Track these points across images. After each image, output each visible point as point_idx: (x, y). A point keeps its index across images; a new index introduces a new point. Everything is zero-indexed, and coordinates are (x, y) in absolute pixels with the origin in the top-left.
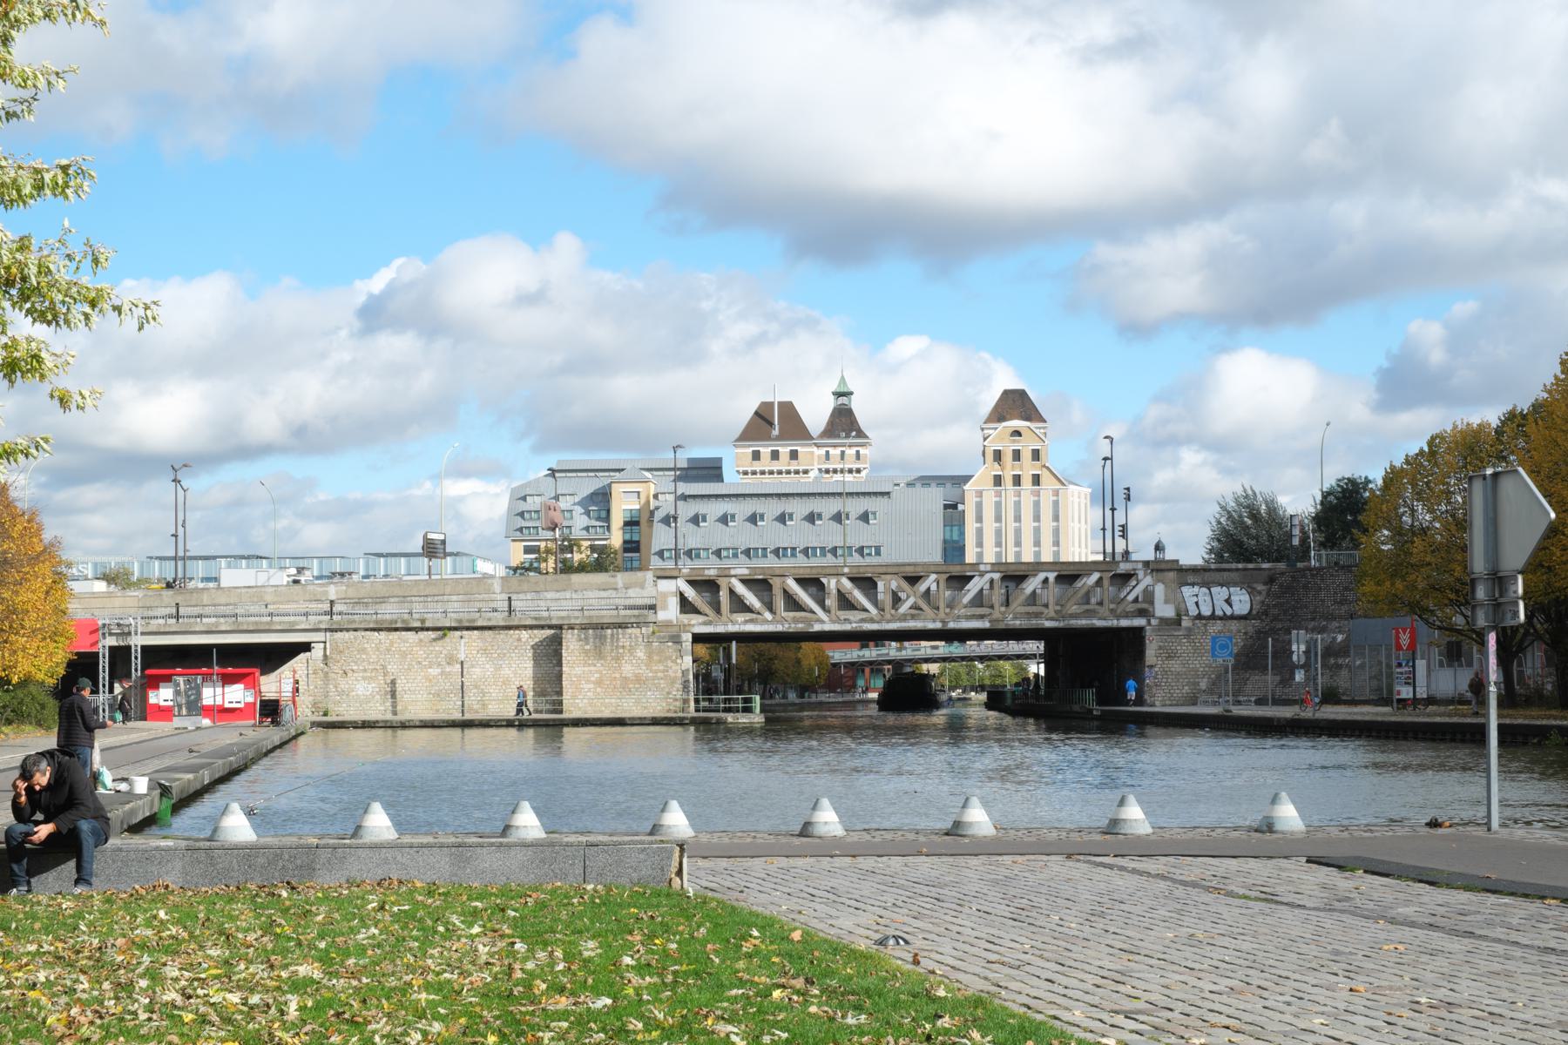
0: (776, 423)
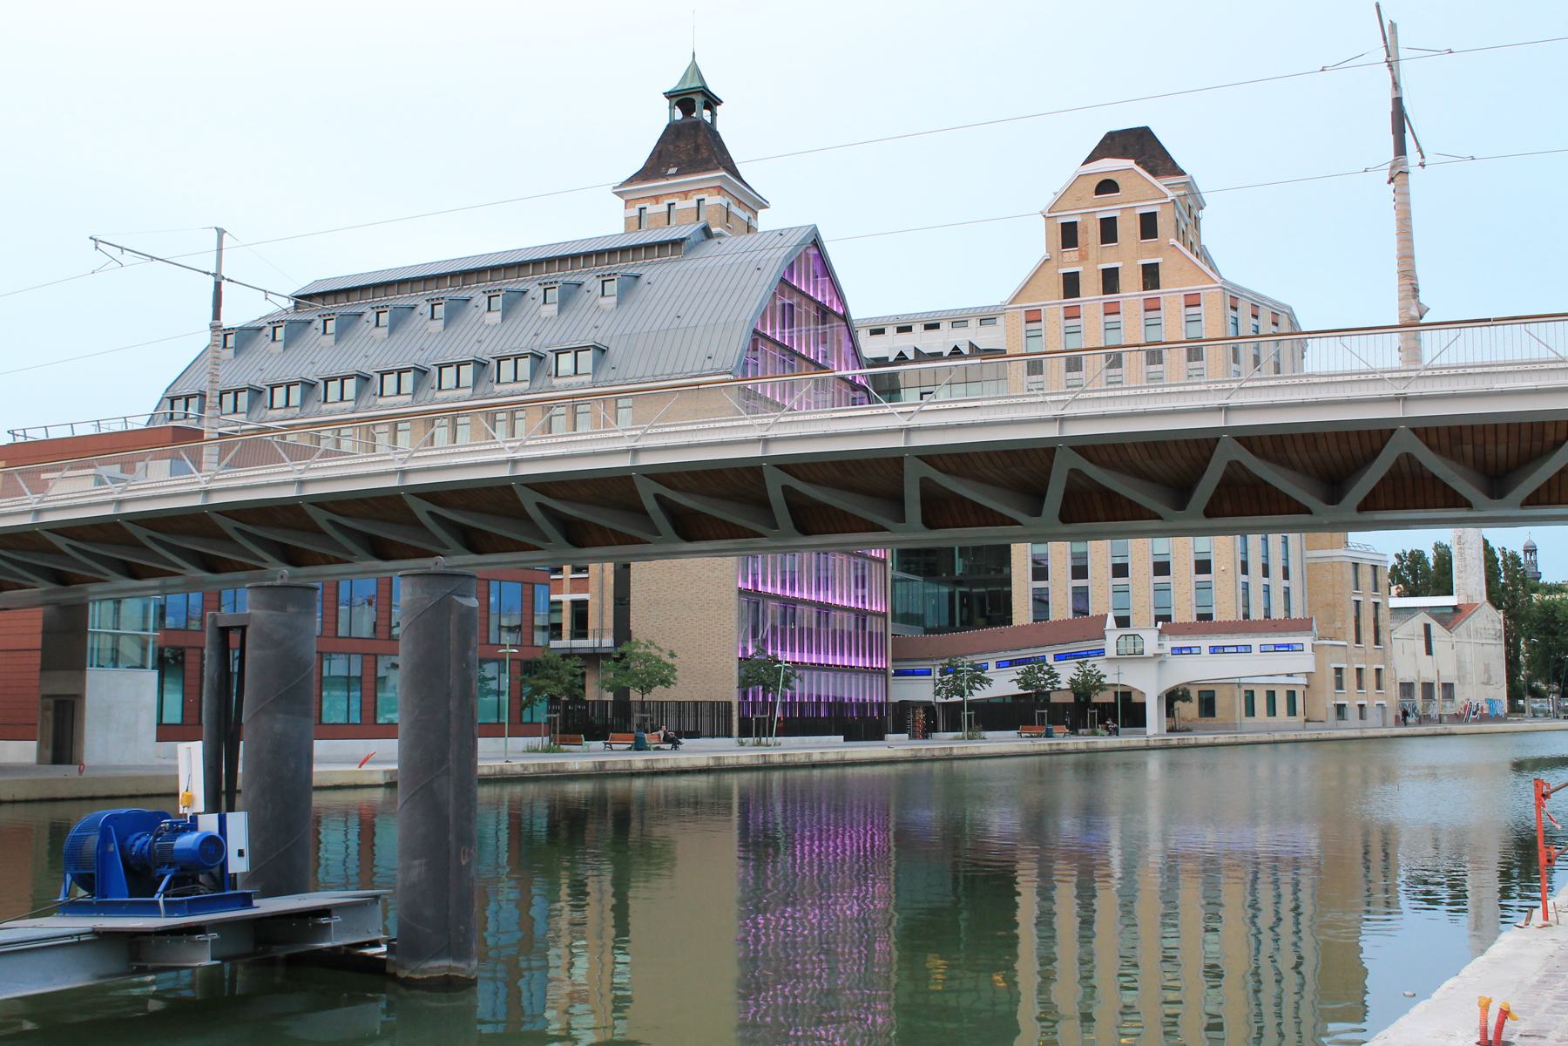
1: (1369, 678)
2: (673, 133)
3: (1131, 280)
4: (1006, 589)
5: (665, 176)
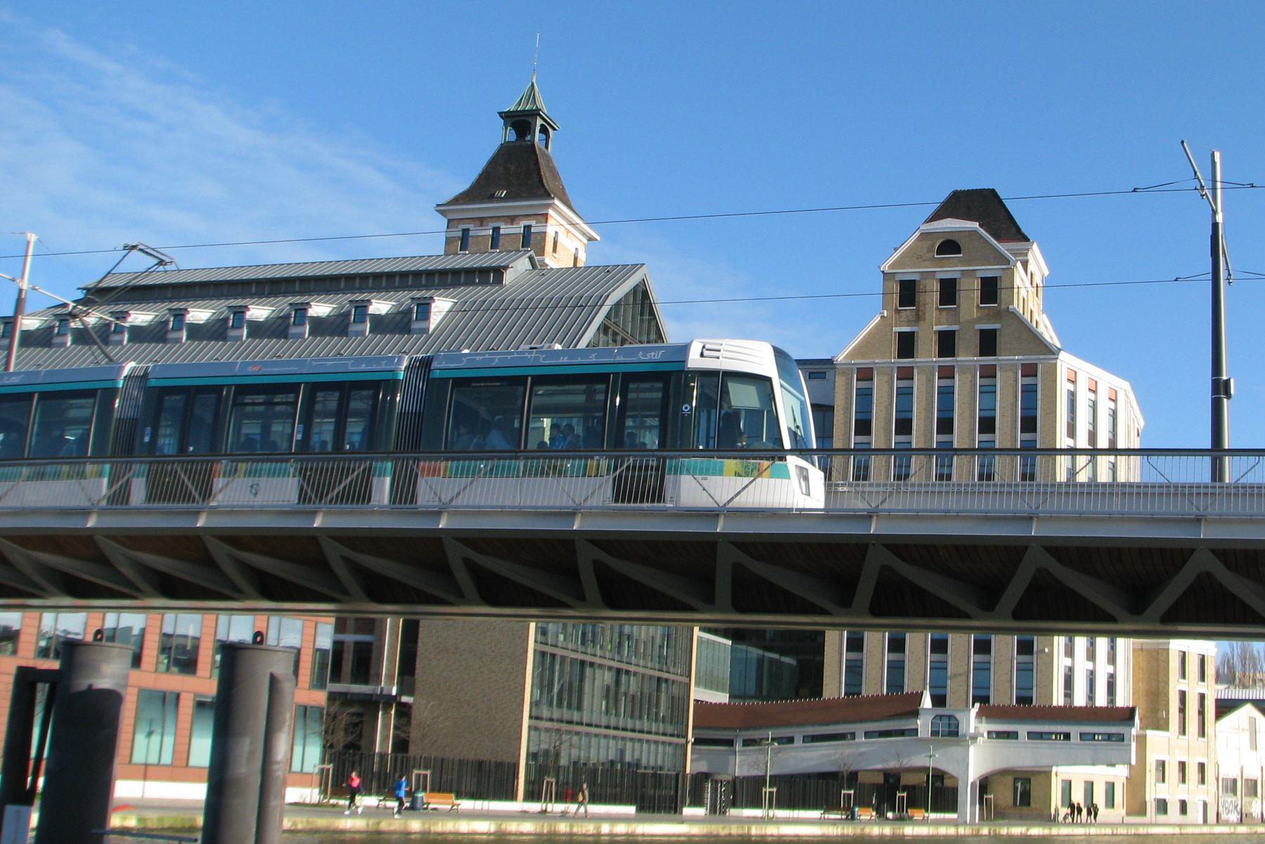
1: (1192, 772)
2: (505, 155)
4: (817, 658)
5: (491, 198)
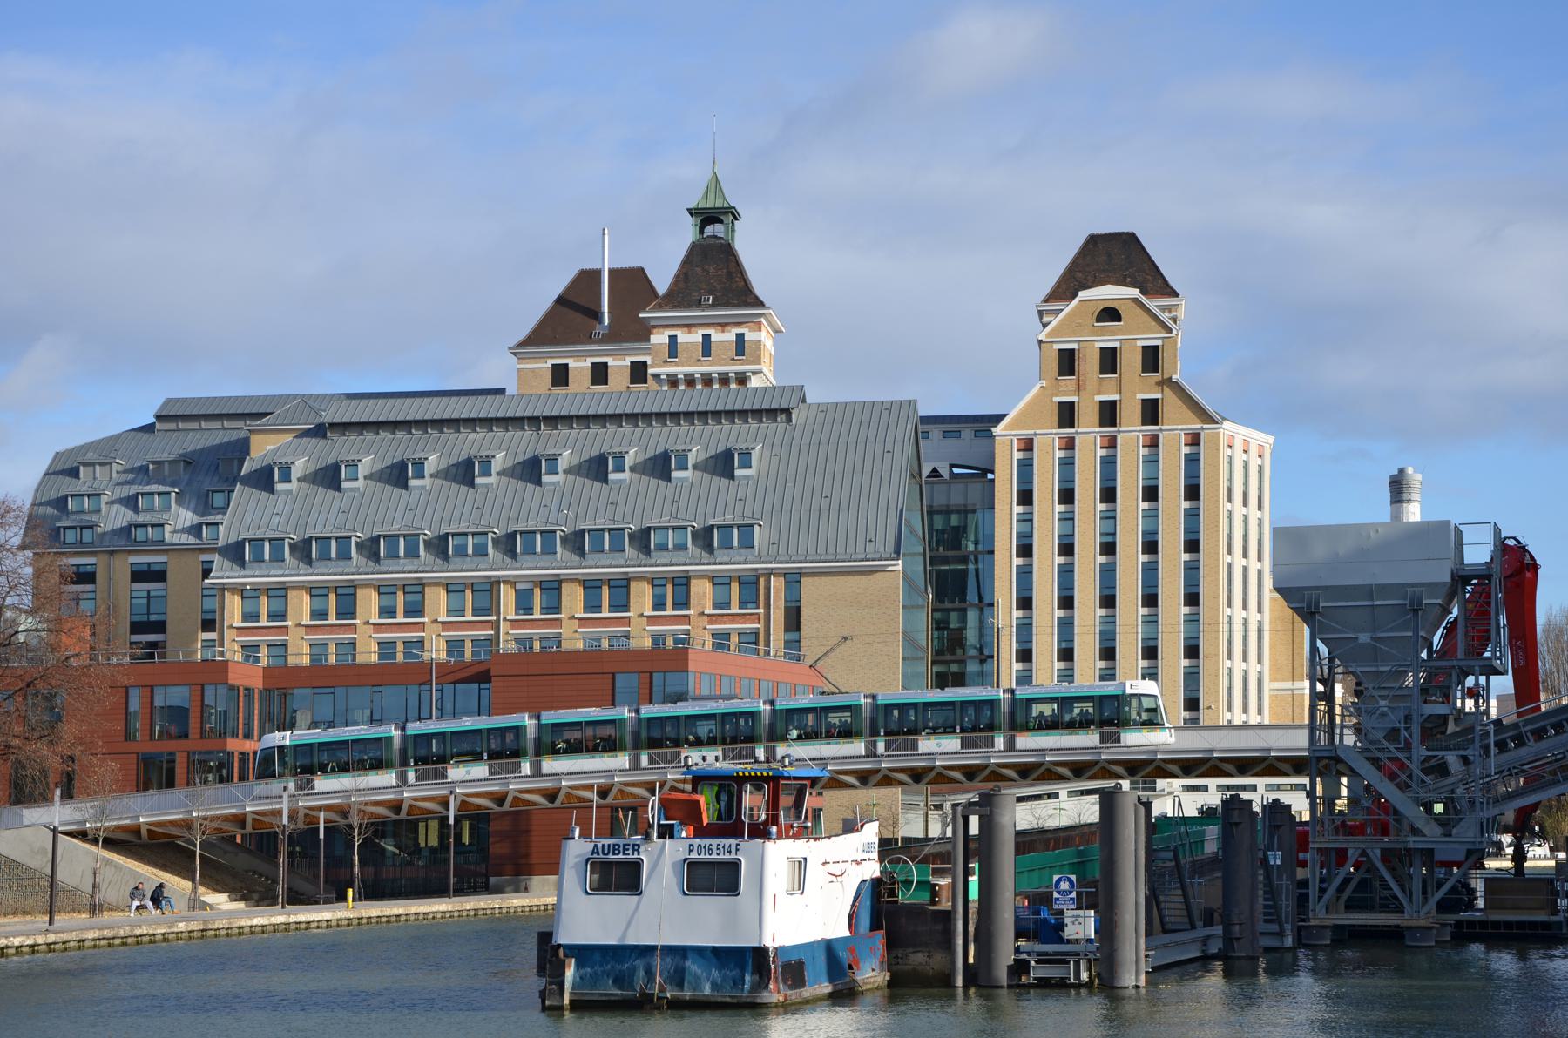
0: (606, 309)
3: (1130, 413)
